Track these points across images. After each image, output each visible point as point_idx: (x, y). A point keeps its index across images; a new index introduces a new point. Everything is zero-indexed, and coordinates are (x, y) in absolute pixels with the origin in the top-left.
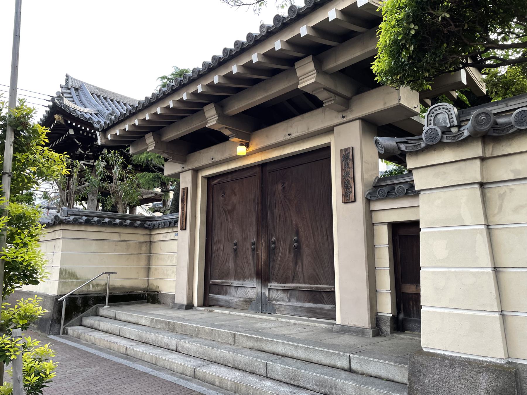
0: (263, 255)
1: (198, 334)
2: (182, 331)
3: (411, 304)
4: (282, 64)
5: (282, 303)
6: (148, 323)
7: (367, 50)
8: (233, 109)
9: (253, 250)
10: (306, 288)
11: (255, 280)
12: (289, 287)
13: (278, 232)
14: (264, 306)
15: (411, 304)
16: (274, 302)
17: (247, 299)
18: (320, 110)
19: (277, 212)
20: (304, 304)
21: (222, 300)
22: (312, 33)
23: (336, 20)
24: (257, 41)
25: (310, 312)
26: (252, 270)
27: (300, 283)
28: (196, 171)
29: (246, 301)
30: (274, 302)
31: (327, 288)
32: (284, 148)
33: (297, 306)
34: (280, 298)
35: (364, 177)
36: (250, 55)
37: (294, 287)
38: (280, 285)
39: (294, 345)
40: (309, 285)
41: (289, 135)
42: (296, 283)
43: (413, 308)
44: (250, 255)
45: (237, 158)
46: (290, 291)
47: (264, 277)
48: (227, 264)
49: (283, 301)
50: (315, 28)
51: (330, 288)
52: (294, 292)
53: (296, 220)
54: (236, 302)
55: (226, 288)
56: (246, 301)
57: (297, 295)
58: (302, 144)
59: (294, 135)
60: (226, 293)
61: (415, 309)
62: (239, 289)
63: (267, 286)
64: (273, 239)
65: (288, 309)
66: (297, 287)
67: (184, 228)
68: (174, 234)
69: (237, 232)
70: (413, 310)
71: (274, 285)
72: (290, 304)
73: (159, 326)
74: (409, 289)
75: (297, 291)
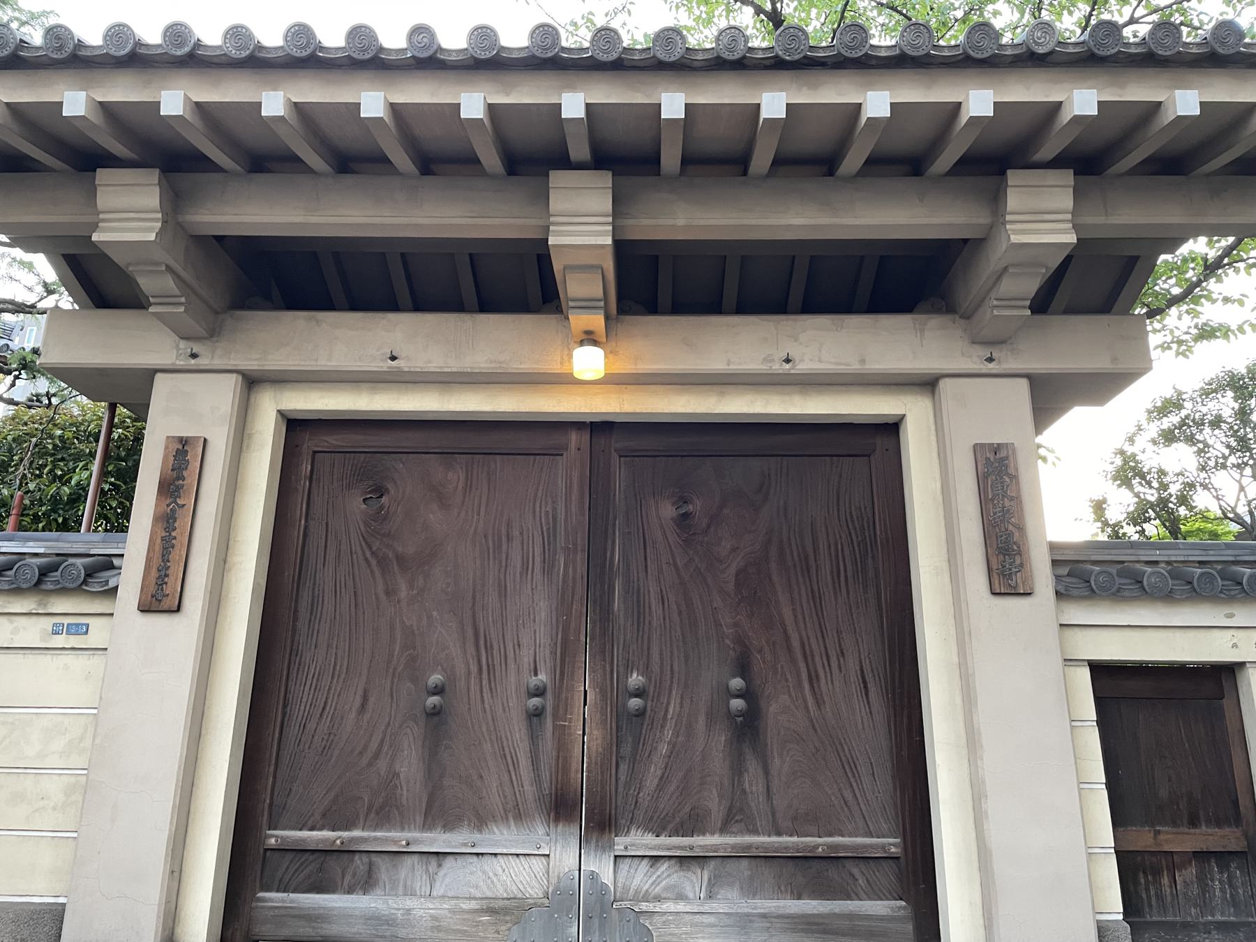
3: (1142, 881)
4: (531, 155)
5: (681, 907)
7: (314, 219)
8: (661, 222)
9: (536, 715)
11: (541, 830)
12: (715, 848)
15: (1142, 881)
16: (644, 906)
17: (497, 904)
18: (950, 317)
19: (653, 589)
20: (782, 903)
21: (346, 916)
22: (96, 118)
23: (281, 119)
24: (19, 57)
26: (529, 789)
27: (755, 832)
28: (252, 382)
29: (491, 911)
31: (871, 846)
32: (722, 394)
33: (748, 915)
34: (666, 889)
36: (871, 86)
37: (734, 847)
38: (664, 840)
40: (795, 839)
41: (788, 361)
42: (740, 832)
43: (1147, 890)
44: (518, 734)
45: (566, 380)
46: (713, 863)
47: (592, 812)
48: (382, 765)
49: (681, 897)
50: (299, 109)
51: (883, 847)
52: (731, 866)
53: (736, 625)
54: (434, 918)
55: (371, 864)
56: (491, 911)
57: (747, 873)
60: (366, 883)
61: (1152, 892)
62: (449, 862)
63: (611, 846)
64: (635, 679)
66: (749, 847)
67: (161, 599)
68: (48, 623)
69: (447, 644)
70: (1149, 897)
72: (717, 906)
75: (745, 863)
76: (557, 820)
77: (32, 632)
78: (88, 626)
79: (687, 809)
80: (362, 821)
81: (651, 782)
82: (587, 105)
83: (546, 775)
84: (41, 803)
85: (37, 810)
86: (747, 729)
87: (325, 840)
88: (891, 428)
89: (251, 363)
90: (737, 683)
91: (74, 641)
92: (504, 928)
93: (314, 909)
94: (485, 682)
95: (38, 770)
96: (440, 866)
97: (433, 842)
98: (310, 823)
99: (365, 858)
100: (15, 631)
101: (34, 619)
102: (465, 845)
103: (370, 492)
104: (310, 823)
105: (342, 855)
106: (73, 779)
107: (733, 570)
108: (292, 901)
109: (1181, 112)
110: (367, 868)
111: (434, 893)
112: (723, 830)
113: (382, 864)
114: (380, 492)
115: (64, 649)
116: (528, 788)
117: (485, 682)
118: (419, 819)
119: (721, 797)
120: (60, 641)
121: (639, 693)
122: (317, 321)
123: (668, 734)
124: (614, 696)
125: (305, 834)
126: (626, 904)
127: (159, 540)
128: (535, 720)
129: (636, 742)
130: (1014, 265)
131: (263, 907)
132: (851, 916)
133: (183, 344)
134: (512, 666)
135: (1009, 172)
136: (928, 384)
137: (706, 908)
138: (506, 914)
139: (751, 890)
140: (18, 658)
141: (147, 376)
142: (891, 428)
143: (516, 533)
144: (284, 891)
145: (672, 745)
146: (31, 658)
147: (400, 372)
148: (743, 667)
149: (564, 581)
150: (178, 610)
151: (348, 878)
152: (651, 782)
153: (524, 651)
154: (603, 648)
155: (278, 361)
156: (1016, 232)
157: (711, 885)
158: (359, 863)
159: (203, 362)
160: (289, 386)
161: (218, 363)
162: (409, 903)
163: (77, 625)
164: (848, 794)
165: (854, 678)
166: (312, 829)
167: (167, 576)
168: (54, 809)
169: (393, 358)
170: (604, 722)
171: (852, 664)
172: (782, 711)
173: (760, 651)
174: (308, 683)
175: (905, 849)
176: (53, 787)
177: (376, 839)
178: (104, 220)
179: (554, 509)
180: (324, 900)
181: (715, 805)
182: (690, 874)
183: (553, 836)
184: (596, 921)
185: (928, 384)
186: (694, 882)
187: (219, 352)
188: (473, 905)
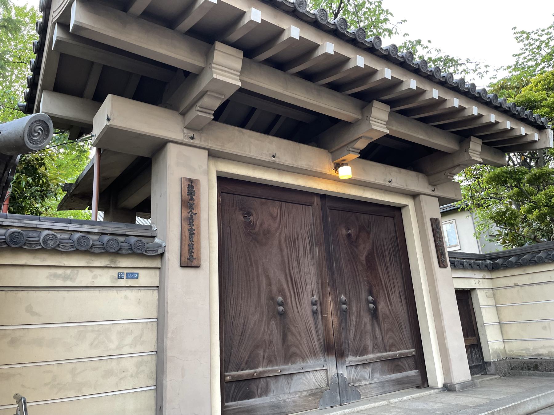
0: (332, 319)
7: (286, 93)
9: (315, 313)
10: (390, 356)
12: (372, 359)
13: (347, 288)
16: (357, 384)
25: (398, 384)
29: (312, 395)
31: (408, 353)
33: (384, 382)
39: (535, 399)
40: (390, 353)
46: (371, 365)
47: (334, 349)
54: (294, 402)
56: (312, 395)
58: (383, 195)
59: (394, 184)
60: (266, 391)
62: (295, 377)
65: (375, 387)
71: (351, 359)
74: (472, 340)
76: (328, 355)
77: (105, 278)
78: (138, 274)
79: (362, 346)
80: (261, 363)
81: (352, 336)
84: (123, 374)
85: (121, 379)
86: (374, 314)
87: (249, 375)
88: (398, 209)
89: (216, 146)
90: (370, 298)
91: (130, 283)
92: (317, 401)
93: (249, 407)
94: (297, 300)
95: (117, 357)
96: (292, 379)
97: (289, 369)
98: (241, 367)
99: (264, 380)
100: (95, 277)
101: (106, 270)
102: (300, 369)
103: (245, 214)
104: (241, 367)
105: (256, 380)
106: (140, 359)
107: (364, 256)
108: (240, 405)
110: (265, 385)
111: (291, 391)
113: (272, 382)
114: (249, 214)
115: (125, 287)
116: (317, 343)
117: (297, 300)
118: (282, 361)
119: (371, 340)
120: (123, 282)
121: (345, 303)
122: (243, 133)
123: (354, 319)
124: (338, 303)
125: (240, 373)
126: (352, 384)
127: (187, 231)
128: (315, 315)
129: (346, 322)
130: (463, 165)
131: (228, 410)
132: (407, 377)
133: (186, 131)
134: (305, 293)
136: (414, 196)
137: (373, 382)
138: (317, 395)
139: (382, 373)
140: (96, 293)
141: (160, 146)
142: (398, 209)
143: (300, 236)
144: (235, 401)
145: (356, 322)
146: (104, 293)
147: (275, 163)
148: (371, 293)
149: (319, 258)
150: (181, 266)
151: (259, 390)
152: (352, 336)
153: (308, 287)
154: (334, 286)
155: (229, 148)
157: (372, 373)
158: (262, 382)
159: (196, 142)
160: (220, 159)
161: (203, 144)
162: (285, 397)
163: (132, 274)
164: (401, 336)
165: (398, 294)
166: (242, 370)
167: (193, 249)
168: (132, 376)
169: (274, 157)
170: (337, 315)
171: (397, 291)
172: (382, 307)
173: (375, 286)
174: (232, 302)
175: (416, 353)
176: (129, 364)
177: (269, 371)
178: (215, 68)
179: (311, 228)
180: (253, 402)
181: (369, 343)
182: (366, 370)
183: (328, 361)
184: (344, 392)
185: (414, 196)
186: (366, 372)
187: (203, 139)
188: (304, 394)
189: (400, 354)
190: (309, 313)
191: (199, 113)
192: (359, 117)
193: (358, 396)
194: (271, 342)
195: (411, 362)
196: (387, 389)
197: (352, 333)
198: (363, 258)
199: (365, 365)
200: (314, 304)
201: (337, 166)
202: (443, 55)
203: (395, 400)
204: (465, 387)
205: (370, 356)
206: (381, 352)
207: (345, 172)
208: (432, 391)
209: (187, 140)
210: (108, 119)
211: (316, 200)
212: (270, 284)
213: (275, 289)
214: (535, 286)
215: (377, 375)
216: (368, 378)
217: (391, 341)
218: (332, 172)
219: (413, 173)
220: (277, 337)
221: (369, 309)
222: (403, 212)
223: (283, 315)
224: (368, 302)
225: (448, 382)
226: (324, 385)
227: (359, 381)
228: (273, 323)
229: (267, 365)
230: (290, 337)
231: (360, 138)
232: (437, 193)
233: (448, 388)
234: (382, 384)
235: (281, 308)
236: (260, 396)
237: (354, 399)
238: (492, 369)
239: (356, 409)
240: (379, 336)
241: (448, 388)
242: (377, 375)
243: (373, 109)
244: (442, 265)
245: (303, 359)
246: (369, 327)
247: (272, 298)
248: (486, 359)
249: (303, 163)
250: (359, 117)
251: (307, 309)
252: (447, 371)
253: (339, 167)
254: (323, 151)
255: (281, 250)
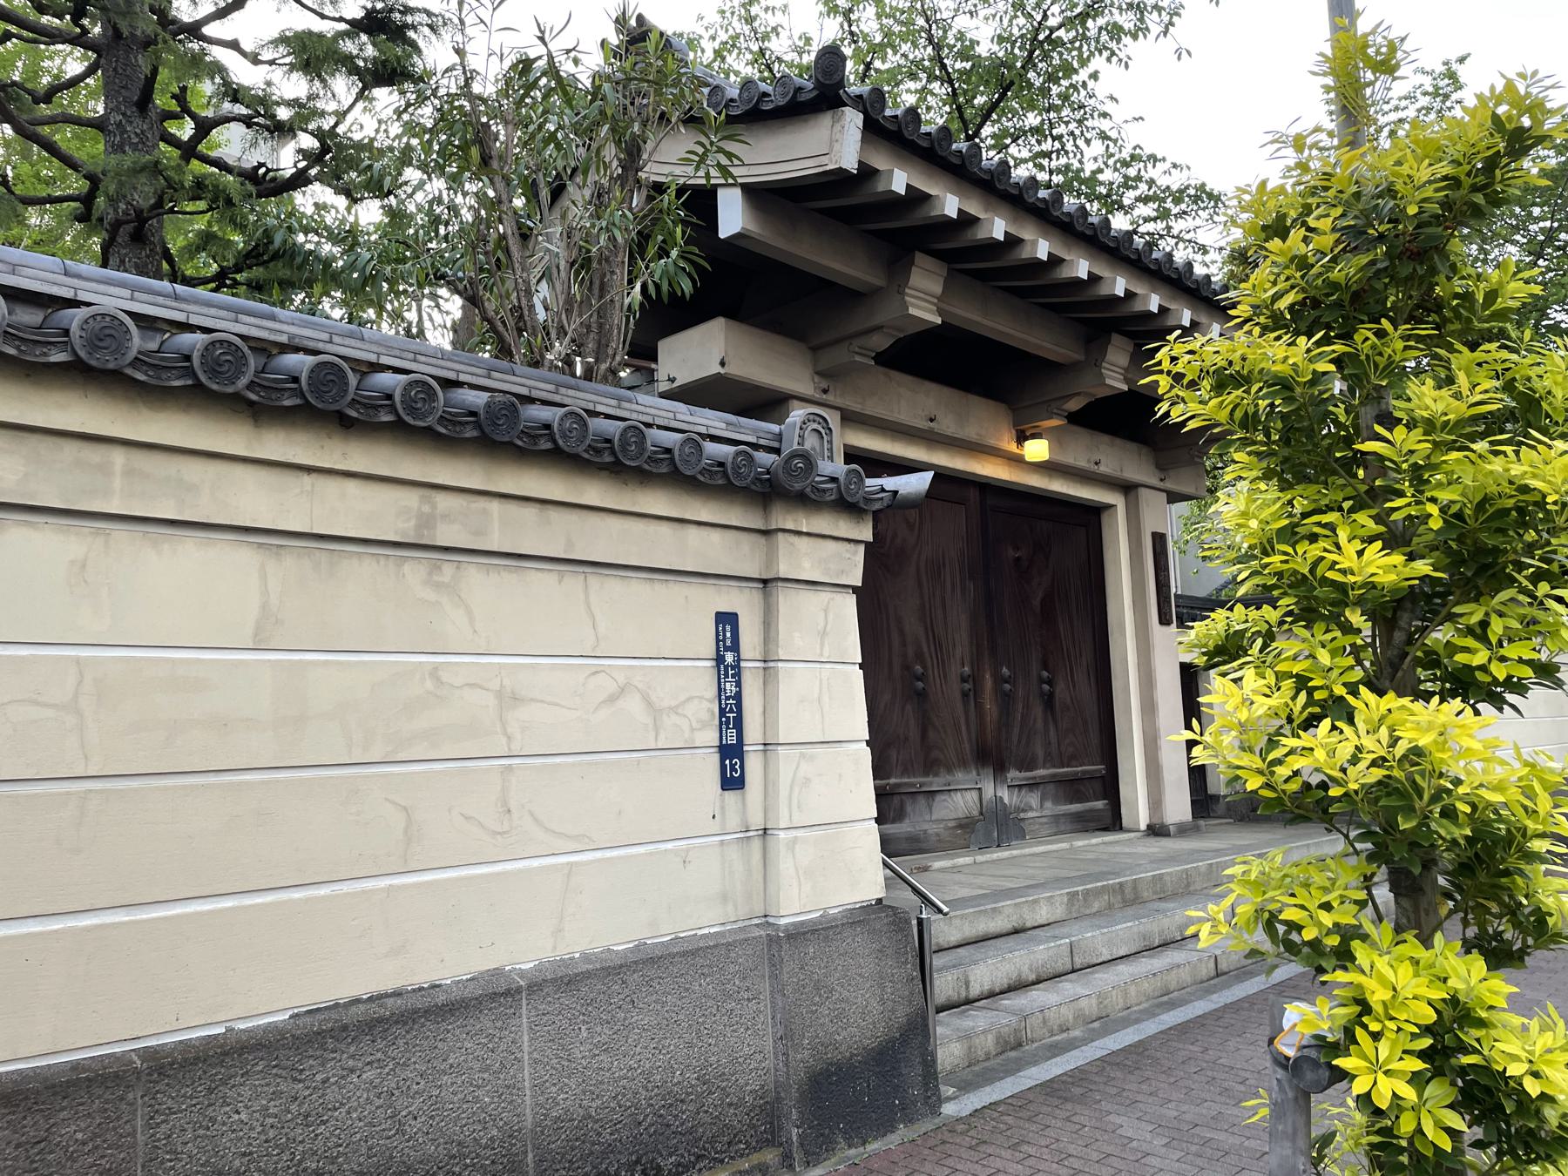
1: (1188, 885)
2: (1155, 893)
6: (1059, 912)
7: (985, 322)
9: (965, 695)
14: (995, 827)
16: (1022, 815)
29: (960, 826)
30: (1022, 815)
35: (1175, 588)
38: (1023, 774)
56: (960, 826)
59: (1103, 469)
62: (939, 798)
71: (1013, 774)
73: (1096, 906)
81: (1015, 739)
82: (908, 185)
83: (974, 736)
86: (1049, 701)
88: (1094, 514)
90: (1045, 674)
109: (946, 212)
112: (1044, 767)
124: (999, 680)
133: (817, 379)
135: (919, 257)
136: (1128, 489)
139: (1056, 801)
142: (1094, 514)
147: (931, 431)
152: (1015, 739)
155: (873, 408)
156: (914, 306)
181: (1040, 753)
186: (1033, 799)
188: (951, 824)
189: (1084, 772)
190: (958, 695)
191: (858, 358)
192: (1081, 357)
193: (1021, 835)
194: (907, 739)
195: (1098, 786)
196: (1063, 828)
197: (1016, 731)
198: (1036, 602)
199: (1032, 786)
200: (964, 680)
201: (1021, 438)
202: (1195, 177)
203: (1080, 843)
204: (1183, 830)
205: (1041, 772)
206: (1054, 767)
207: (1037, 450)
208: (1132, 835)
209: (818, 396)
210: (722, 364)
211: (973, 495)
212: (904, 644)
213: (911, 652)
214: (504, 574)
215: (1048, 804)
216: (1037, 808)
217: (1071, 749)
218: (1013, 447)
219: (1133, 446)
220: (914, 733)
221: (1042, 694)
222: (1105, 518)
223: (922, 696)
224: (1042, 681)
225: (1155, 821)
226: (976, 813)
227: (1024, 811)
228: (909, 707)
229: (902, 775)
230: (931, 734)
231: (1078, 394)
232: (1169, 485)
233: (1156, 830)
234: (1056, 818)
235: (920, 685)
236: (893, 822)
237: (1017, 838)
238: (1220, 808)
239: (1027, 851)
240: (1053, 739)
241: (1156, 830)
242: (1048, 804)
243: (1110, 349)
244: (1164, 620)
245: (949, 770)
246: (1040, 724)
247: (907, 667)
248: (1211, 790)
249: (970, 432)
250: (1081, 357)
251: (955, 689)
252: (1156, 803)
253: (1026, 439)
254: (1002, 407)
255: (920, 585)
